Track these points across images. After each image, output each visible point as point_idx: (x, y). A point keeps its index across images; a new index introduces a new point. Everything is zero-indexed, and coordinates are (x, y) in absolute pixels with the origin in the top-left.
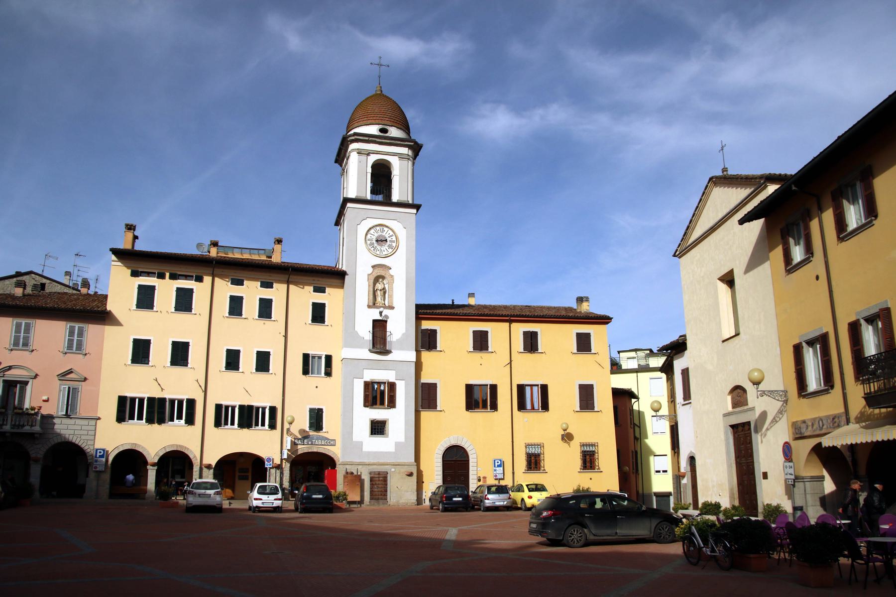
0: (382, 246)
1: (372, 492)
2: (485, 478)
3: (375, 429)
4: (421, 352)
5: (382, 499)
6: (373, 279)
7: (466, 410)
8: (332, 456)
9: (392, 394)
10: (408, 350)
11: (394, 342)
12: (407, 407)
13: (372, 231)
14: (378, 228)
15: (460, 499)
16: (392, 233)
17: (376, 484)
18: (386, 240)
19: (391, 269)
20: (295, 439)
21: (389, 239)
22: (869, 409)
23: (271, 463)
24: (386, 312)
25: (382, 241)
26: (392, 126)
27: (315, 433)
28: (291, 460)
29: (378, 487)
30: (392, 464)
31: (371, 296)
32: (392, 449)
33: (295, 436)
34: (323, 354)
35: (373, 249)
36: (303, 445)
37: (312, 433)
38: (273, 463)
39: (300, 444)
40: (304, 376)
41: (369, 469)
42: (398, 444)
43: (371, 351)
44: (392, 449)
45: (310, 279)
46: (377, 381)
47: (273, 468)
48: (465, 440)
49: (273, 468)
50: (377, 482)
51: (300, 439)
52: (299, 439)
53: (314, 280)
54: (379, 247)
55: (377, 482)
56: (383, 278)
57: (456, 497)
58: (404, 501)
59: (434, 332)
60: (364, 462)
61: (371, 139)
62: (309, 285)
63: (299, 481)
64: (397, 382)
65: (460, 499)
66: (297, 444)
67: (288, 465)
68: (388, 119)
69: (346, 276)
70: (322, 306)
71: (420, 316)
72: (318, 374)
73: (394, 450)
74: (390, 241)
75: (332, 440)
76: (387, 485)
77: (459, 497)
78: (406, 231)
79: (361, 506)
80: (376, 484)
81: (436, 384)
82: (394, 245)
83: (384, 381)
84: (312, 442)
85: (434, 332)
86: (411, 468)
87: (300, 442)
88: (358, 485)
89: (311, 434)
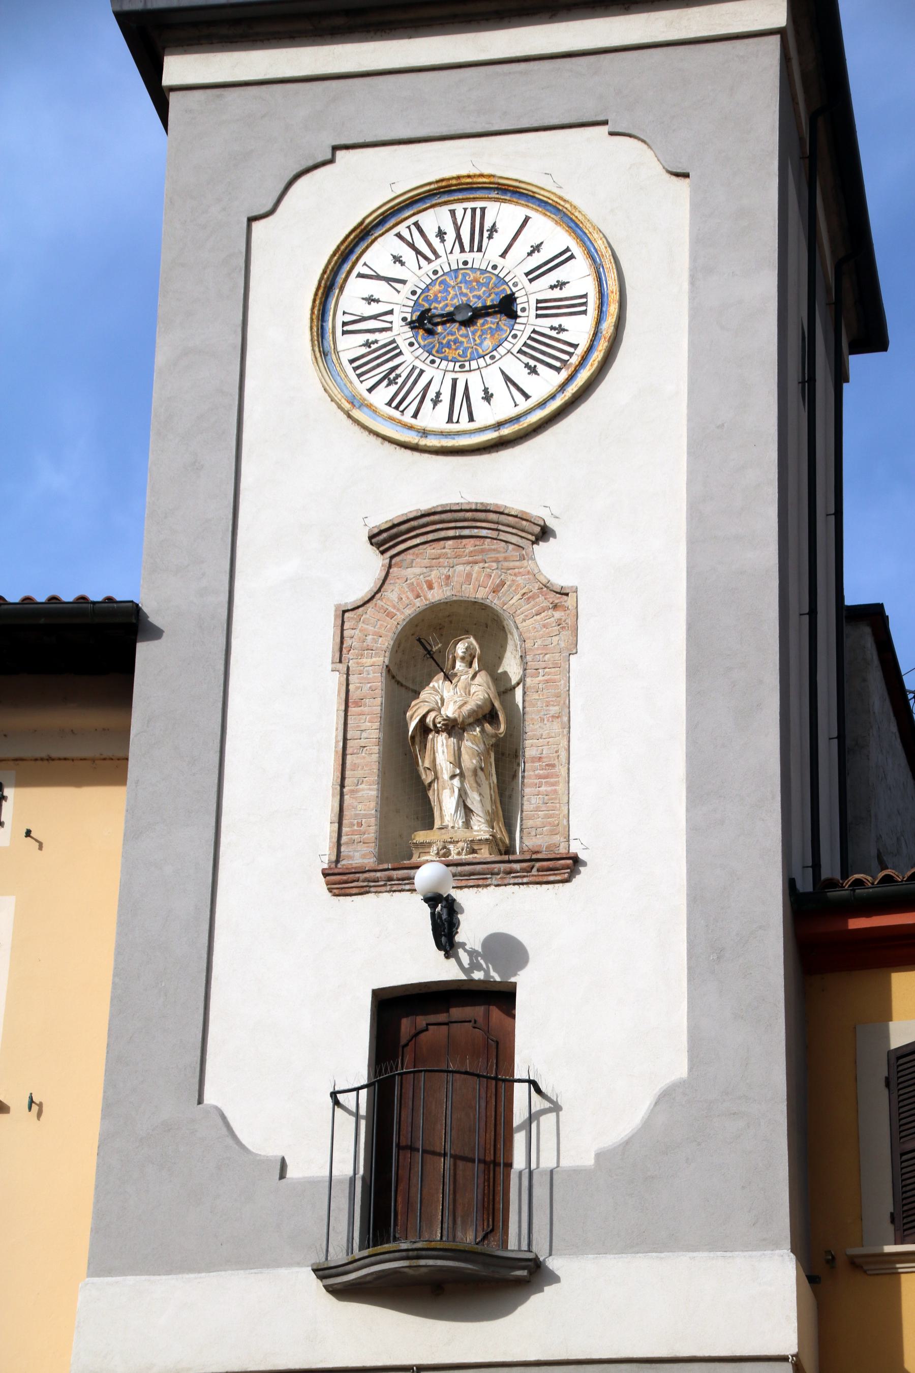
0: (463, 362)
6: (386, 642)
11: (576, 1172)
19: (544, 533)
22: (477, 326)
35: (384, 393)
69: (143, 650)
71: (856, 923)
74: (544, 308)
78: (694, 191)
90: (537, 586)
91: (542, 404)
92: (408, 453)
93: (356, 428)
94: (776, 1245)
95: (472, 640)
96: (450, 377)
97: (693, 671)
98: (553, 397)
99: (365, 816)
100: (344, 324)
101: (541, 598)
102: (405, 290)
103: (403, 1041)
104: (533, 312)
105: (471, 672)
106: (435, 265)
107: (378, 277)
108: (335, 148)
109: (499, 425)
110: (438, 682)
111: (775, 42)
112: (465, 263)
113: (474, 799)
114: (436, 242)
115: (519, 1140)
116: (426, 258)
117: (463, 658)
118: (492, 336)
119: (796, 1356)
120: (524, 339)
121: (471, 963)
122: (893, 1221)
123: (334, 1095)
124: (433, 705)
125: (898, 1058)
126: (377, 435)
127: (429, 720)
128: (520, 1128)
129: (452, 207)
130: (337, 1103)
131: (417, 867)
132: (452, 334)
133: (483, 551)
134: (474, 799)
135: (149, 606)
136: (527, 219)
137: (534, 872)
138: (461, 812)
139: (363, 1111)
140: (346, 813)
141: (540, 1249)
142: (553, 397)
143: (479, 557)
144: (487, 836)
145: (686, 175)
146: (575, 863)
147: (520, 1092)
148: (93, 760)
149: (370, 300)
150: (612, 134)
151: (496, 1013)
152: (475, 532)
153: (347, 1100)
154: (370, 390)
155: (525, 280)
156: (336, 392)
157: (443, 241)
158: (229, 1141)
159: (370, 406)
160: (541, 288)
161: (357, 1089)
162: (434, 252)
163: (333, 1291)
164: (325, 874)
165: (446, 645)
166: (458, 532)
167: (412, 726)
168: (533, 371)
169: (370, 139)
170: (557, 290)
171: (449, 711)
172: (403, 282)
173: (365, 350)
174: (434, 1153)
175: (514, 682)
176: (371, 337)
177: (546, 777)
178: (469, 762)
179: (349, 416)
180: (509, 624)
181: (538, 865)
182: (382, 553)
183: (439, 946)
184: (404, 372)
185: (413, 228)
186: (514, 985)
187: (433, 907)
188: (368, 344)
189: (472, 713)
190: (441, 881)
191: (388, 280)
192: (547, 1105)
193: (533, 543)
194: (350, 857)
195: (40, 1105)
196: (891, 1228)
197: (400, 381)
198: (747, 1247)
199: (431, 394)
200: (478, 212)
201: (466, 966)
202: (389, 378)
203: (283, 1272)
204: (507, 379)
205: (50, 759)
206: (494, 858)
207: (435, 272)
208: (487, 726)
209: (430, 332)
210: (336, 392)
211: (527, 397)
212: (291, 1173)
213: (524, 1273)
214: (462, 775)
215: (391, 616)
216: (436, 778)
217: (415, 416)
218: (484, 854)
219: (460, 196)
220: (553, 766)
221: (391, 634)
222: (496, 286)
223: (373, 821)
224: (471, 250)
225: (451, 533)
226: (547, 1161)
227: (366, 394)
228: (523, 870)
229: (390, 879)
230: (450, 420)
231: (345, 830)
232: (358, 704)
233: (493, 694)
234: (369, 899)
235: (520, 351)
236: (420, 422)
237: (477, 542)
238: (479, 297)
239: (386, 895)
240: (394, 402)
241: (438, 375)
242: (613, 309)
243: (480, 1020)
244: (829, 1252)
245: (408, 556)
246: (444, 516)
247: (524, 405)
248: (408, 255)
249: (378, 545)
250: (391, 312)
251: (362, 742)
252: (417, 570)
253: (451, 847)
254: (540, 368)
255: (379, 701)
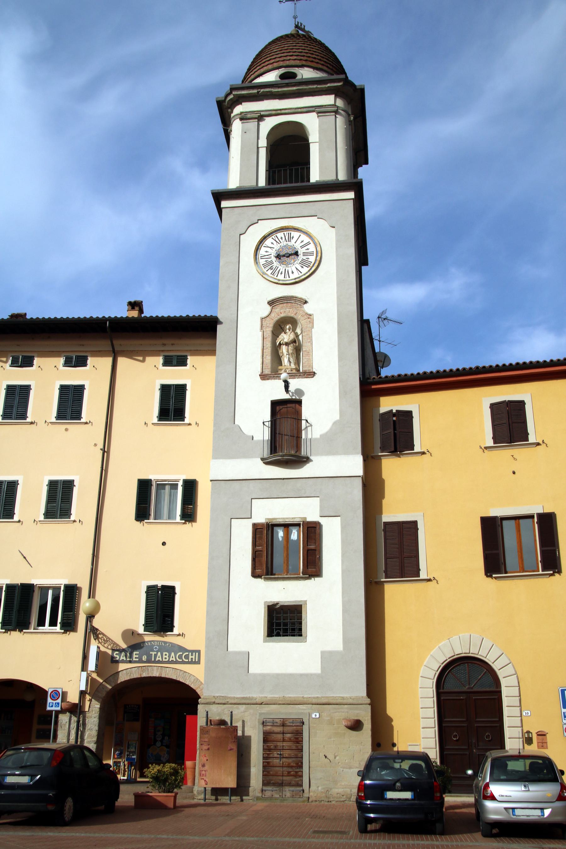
0: (287, 264)
1: (267, 767)
2: (542, 735)
3: (278, 624)
4: (381, 459)
5: (290, 785)
6: (272, 325)
7: (487, 576)
8: (192, 686)
9: (312, 547)
10: (347, 452)
11: (316, 439)
12: (345, 572)
13: (268, 242)
14: (280, 235)
15: (407, 795)
16: (306, 239)
17: (276, 748)
18: (296, 254)
19: (306, 302)
20: (113, 650)
21: (301, 251)
23: (59, 701)
24: (295, 384)
25: (289, 256)
26: (302, 66)
27: (157, 638)
28: (104, 694)
29: (281, 757)
30: (314, 701)
31: (268, 358)
32: (315, 667)
33: (115, 643)
34: (180, 477)
35: (270, 271)
36: (130, 662)
37: (149, 638)
38: (62, 701)
39: (123, 661)
40: (138, 523)
41: (261, 714)
42: (326, 656)
43: (267, 462)
44: (315, 667)
45: (157, 343)
46: (281, 521)
47: (63, 711)
48: (487, 644)
49: (63, 711)
50: (279, 744)
51: (123, 650)
52: (121, 651)
53: (164, 345)
54: (282, 268)
55: (280, 744)
56: (293, 322)
57: (393, 788)
58: (340, 790)
59: (407, 416)
60: (249, 698)
61: (262, 90)
62: (155, 353)
63: (161, 741)
64: (323, 521)
65: (407, 795)
66: (117, 662)
67: (97, 705)
68: (295, 57)
69: (219, 327)
70: (181, 389)
71: (373, 387)
72: (169, 518)
73: (319, 671)
74: (304, 254)
75: (192, 652)
76: (301, 750)
77: (404, 789)
79: (242, 800)
80: (276, 748)
81: (415, 523)
82: (312, 259)
83: (297, 521)
84: (149, 656)
85: (407, 416)
86: (357, 712)
87: (123, 657)
88: (231, 749)
89: (147, 639)
90: (305, 313)
91: (305, 274)
92: (276, 284)
93: (264, 279)
94: (358, 454)
95: (290, 325)
96: (284, 268)
97: (339, 332)
98: (307, 273)
99: (268, 363)
100: (261, 257)
101: (305, 316)
102: (274, 249)
103: (277, 411)
104: (302, 255)
105: (290, 332)
106: (281, 244)
107: (268, 247)
108: (258, 220)
109: (295, 279)
110: (283, 334)
111: (352, 201)
112: (287, 244)
113: (291, 360)
114: (280, 240)
115: (303, 432)
116: (278, 243)
117: (288, 329)
118: (293, 260)
119: (362, 476)
120: (300, 260)
121: (292, 395)
122: (380, 448)
123: (263, 423)
124: (282, 339)
125: (382, 415)
126: (269, 280)
127: (281, 342)
128: (304, 430)
129: (284, 232)
130: (264, 424)
131: (281, 374)
132: (285, 259)
133: (292, 306)
134: (291, 360)
135: (220, 317)
136: (300, 235)
137: (305, 375)
138: (289, 362)
139: (270, 426)
140: (264, 362)
141: (309, 455)
142: (307, 273)
143: (292, 307)
144: (295, 368)
145: (334, 227)
146: (314, 374)
147: (304, 422)
148: (206, 350)
149: (266, 252)
150: (318, 218)
151: (297, 406)
152: (291, 302)
153: (267, 424)
154: (267, 271)
155: (300, 248)
156: (259, 271)
157: (282, 239)
158: (241, 432)
159: (267, 274)
160: (304, 250)
161: (269, 421)
162: (280, 242)
163: (264, 463)
164: (260, 376)
165: (285, 326)
166: (287, 302)
167: (277, 344)
168: (302, 267)
169: (266, 218)
170: (307, 250)
171: (286, 340)
172: (274, 248)
173: (266, 262)
174: (285, 435)
175: (299, 334)
176: (267, 260)
177: (307, 355)
178: (290, 351)
179: (263, 276)
180: (298, 322)
181: (306, 374)
182: (270, 306)
183: (286, 391)
184: (274, 267)
185: (276, 237)
186: (301, 400)
187: (285, 383)
188: (266, 261)
189: (291, 341)
190: (287, 377)
191: (270, 247)
192: (309, 425)
193: (303, 304)
194: (265, 372)
195: (198, 424)
196: (380, 450)
197: (273, 269)
198: (352, 454)
199: (280, 272)
200: (290, 234)
201: (291, 395)
202: (271, 268)
203: (254, 459)
204: (297, 269)
205: (197, 350)
206: (296, 372)
207: (281, 246)
208: (294, 344)
209: (280, 259)
210: (259, 271)
211: (301, 273)
212: (254, 439)
213: (306, 460)
214: (289, 354)
215: (273, 320)
216: (283, 355)
217: (277, 276)
218: (294, 371)
219: (286, 230)
220: (309, 352)
221: (272, 324)
222: (294, 249)
223: (270, 364)
224: (288, 241)
225: (285, 302)
226: (309, 436)
227: (266, 272)
228: (303, 375)
229: (274, 377)
230: (285, 277)
231: (264, 366)
232: (266, 339)
233: (295, 337)
234: (270, 381)
235: (300, 263)
236: (278, 278)
237: (291, 304)
238: (290, 251)
239: (273, 380)
240: (273, 274)
241: (282, 268)
242: (319, 255)
243: (294, 407)
244: (367, 455)
245: (276, 307)
246: (284, 298)
247: (301, 275)
248: (274, 242)
249: (269, 304)
250: (271, 254)
251: (267, 347)
252: (278, 310)
253: (287, 370)
254: (304, 267)
255: (270, 338)
